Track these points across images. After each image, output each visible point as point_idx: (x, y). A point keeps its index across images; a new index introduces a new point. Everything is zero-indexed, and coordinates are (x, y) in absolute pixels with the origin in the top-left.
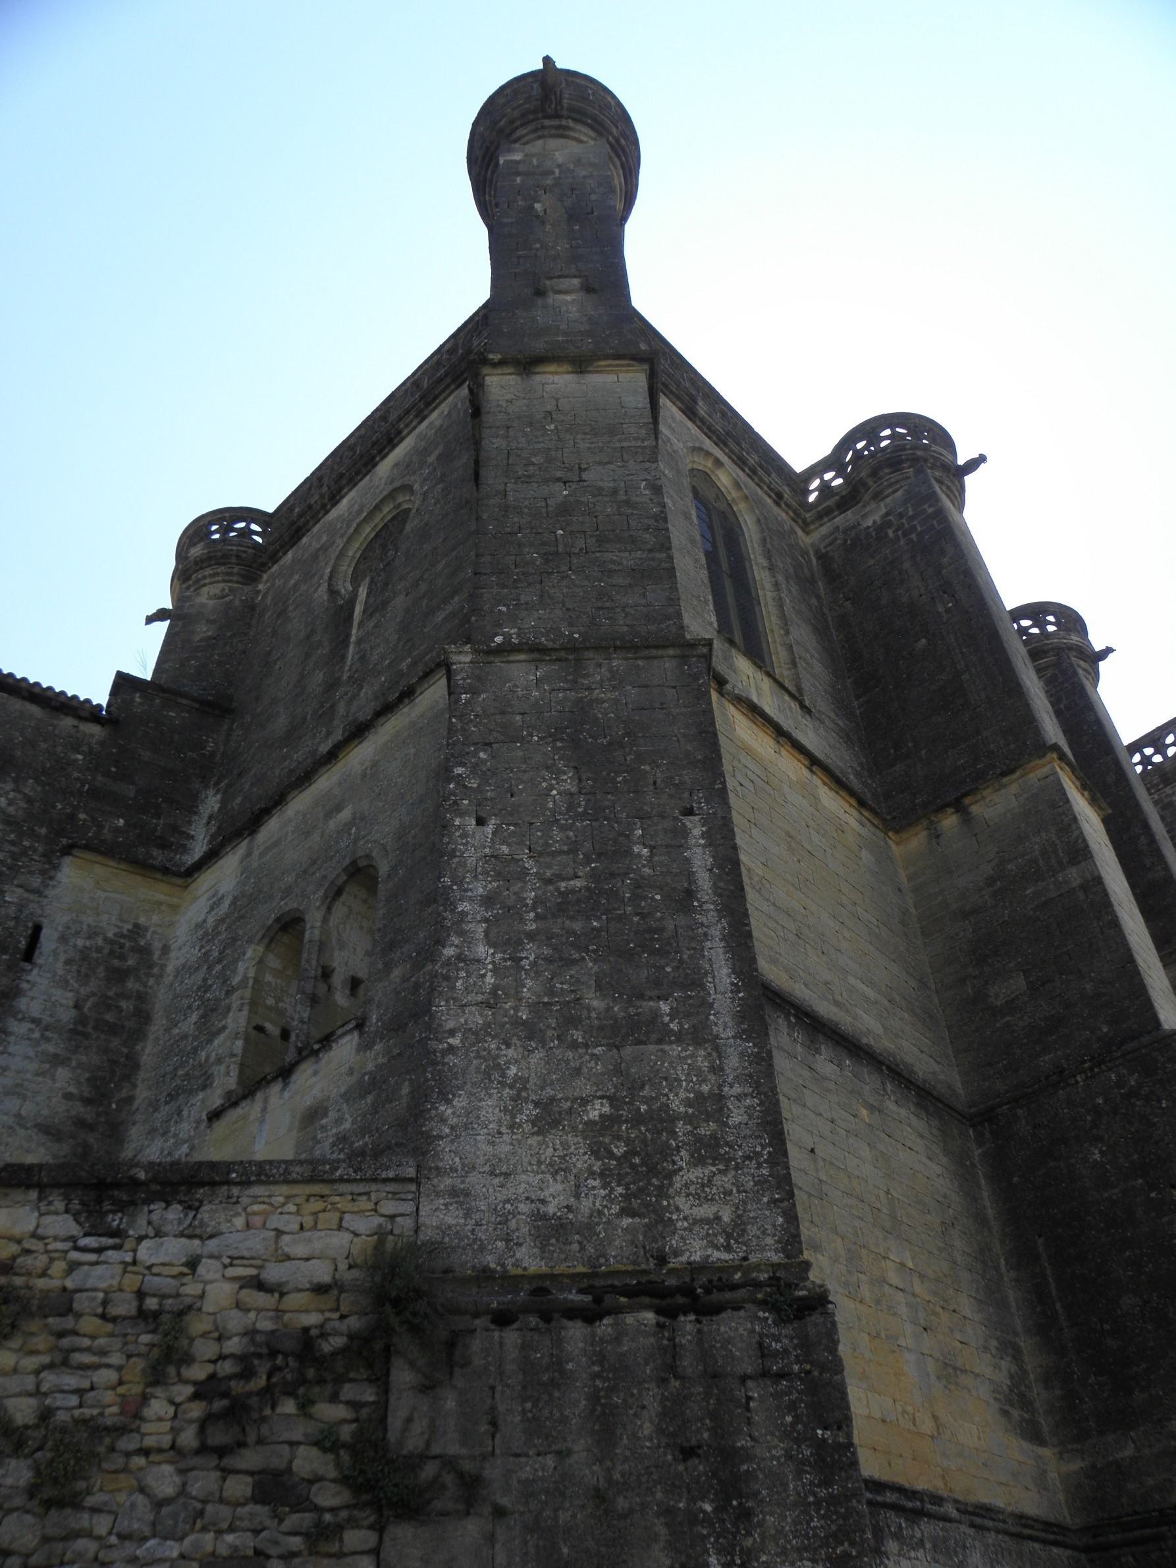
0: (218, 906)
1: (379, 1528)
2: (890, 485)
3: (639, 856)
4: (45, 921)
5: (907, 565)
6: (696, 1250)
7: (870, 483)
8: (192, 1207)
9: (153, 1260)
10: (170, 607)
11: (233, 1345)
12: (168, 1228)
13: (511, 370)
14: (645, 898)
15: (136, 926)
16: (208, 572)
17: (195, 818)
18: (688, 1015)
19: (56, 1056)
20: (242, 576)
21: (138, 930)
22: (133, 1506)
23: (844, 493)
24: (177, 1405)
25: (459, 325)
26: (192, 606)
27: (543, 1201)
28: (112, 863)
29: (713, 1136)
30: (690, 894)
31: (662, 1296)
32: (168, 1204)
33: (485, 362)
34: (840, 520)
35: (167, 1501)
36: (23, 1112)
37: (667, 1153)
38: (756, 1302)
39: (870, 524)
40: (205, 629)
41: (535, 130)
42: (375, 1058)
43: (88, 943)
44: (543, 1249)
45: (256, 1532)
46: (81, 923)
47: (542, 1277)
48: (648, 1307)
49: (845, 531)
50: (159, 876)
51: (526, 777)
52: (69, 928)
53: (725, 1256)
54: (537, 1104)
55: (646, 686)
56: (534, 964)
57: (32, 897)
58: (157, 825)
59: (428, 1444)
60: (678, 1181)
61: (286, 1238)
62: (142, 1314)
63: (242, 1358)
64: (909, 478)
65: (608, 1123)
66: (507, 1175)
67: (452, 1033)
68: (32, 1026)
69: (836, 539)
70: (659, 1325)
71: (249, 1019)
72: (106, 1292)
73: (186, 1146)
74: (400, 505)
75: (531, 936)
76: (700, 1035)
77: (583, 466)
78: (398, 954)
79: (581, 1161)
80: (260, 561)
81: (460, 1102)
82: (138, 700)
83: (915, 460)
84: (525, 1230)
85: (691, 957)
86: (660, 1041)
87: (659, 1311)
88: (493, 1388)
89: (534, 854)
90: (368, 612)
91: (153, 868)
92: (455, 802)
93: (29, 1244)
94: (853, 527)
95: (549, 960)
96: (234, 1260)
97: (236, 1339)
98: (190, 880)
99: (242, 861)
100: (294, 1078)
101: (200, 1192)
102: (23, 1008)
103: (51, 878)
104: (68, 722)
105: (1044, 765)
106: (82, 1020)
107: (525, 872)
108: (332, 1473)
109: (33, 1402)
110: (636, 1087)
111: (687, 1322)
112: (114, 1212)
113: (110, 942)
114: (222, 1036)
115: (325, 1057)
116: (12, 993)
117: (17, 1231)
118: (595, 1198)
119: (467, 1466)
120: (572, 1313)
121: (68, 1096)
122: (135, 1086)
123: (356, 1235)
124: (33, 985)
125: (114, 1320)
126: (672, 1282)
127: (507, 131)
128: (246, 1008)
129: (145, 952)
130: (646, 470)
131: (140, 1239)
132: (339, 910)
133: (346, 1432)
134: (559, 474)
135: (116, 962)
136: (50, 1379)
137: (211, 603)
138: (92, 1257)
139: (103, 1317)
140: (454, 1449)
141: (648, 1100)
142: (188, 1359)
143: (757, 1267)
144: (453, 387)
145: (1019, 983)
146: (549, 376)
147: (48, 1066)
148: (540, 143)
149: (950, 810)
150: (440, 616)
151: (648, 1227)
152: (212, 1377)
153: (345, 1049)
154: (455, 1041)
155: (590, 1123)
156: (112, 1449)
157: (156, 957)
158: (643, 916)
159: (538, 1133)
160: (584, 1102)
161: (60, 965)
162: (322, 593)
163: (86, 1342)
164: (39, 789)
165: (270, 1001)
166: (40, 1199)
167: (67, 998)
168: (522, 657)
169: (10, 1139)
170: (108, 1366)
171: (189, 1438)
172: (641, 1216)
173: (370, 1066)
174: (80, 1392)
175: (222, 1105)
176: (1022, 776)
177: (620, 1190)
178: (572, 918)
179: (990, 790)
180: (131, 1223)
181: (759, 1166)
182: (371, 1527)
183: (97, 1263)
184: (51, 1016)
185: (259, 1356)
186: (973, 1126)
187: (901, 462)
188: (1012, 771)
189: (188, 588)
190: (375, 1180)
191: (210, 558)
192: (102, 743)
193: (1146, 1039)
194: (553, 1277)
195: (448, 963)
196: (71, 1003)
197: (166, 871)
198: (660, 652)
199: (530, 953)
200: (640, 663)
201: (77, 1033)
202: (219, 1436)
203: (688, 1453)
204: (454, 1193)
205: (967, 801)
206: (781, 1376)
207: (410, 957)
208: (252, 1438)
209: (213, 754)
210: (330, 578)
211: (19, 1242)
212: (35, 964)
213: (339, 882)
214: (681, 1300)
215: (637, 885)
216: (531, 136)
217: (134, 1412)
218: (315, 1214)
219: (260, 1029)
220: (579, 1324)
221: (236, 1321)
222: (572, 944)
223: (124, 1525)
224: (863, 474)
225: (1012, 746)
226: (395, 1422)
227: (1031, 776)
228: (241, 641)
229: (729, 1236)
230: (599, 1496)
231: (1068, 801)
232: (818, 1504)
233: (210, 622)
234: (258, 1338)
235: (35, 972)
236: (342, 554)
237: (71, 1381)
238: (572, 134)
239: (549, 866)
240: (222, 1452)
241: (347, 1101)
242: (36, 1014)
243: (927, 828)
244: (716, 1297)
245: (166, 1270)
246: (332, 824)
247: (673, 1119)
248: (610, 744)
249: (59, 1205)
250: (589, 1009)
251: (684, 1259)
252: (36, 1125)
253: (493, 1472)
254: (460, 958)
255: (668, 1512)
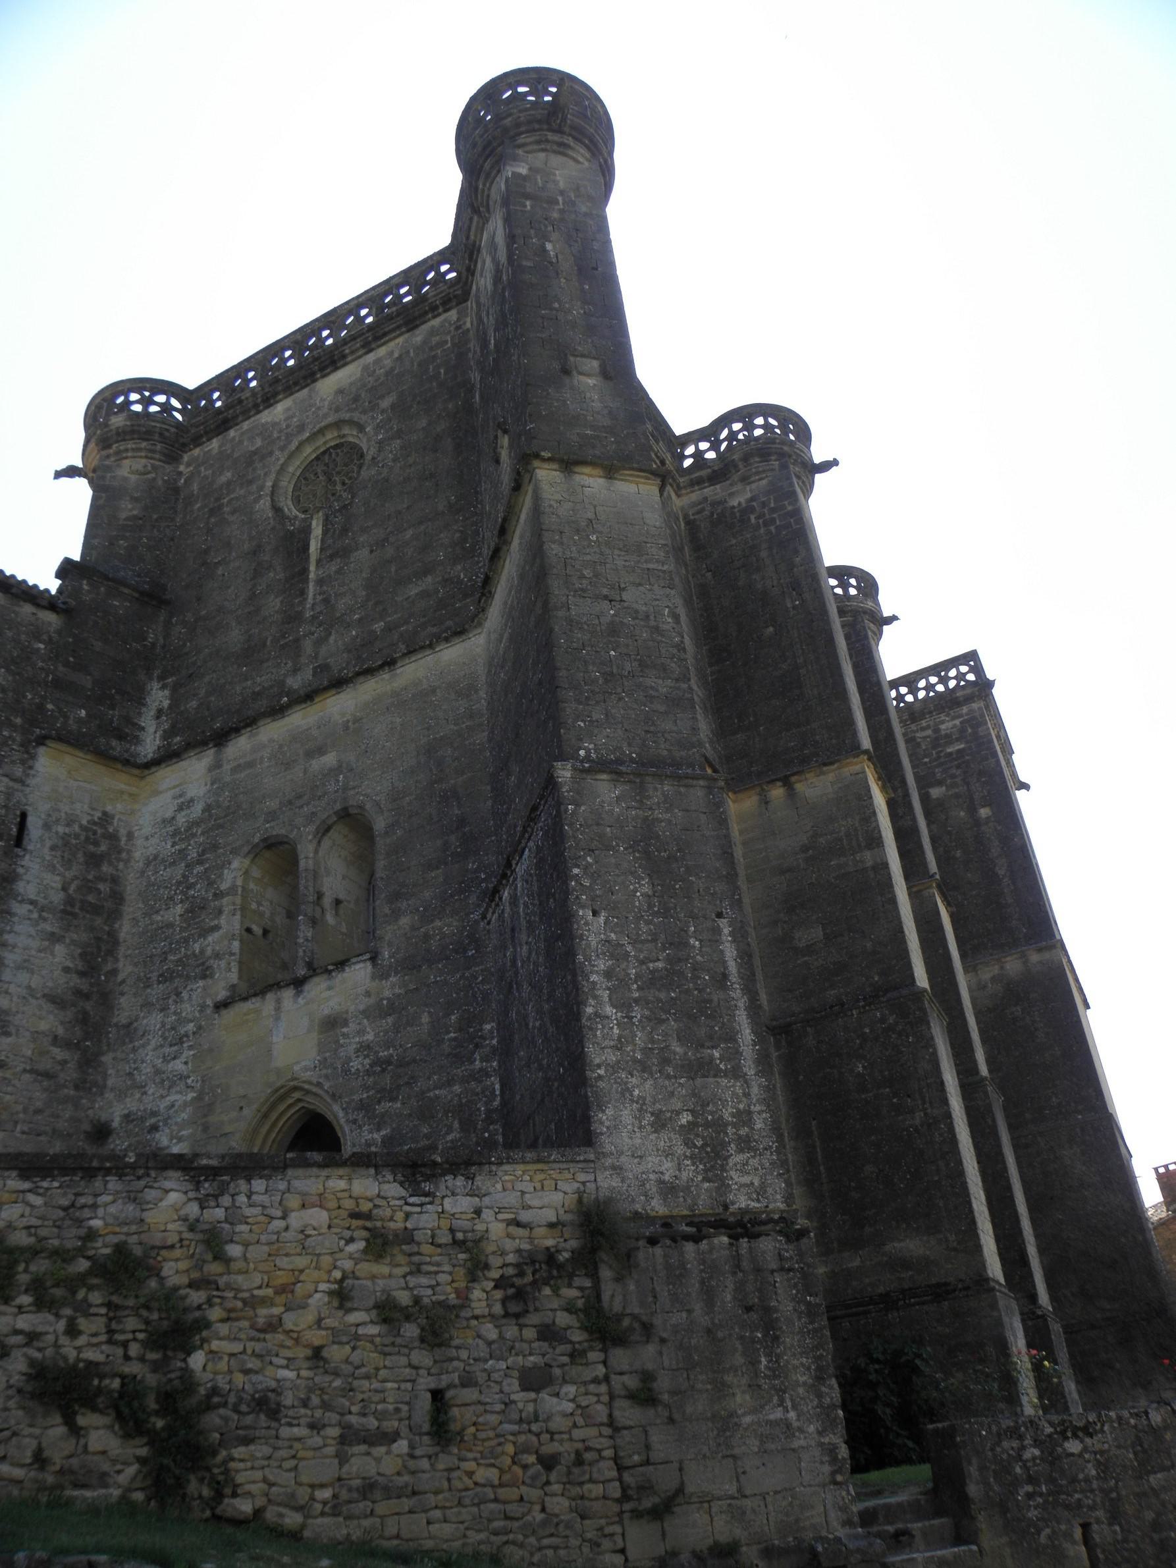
0: (189, 807)
1: (604, 1350)
2: (757, 473)
3: (694, 947)
4: (29, 808)
5: (764, 554)
6: (742, 1201)
7: (741, 466)
8: (470, 1178)
9: (454, 1210)
10: (80, 465)
11: (511, 1258)
12: (458, 1191)
13: (555, 466)
14: (700, 978)
15: (105, 813)
16: (130, 445)
17: (144, 709)
18: (729, 1060)
19: (53, 934)
20: (165, 455)
21: (106, 818)
22: (477, 1345)
23: (716, 468)
24: (487, 1293)
25: (412, 263)
26: (114, 477)
27: (662, 1173)
28: (81, 755)
29: (747, 1136)
30: (725, 976)
31: (731, 1229)
32: (455, 1176)
33: (537, 456)
34: (708, 491)
35: (493, 1342)
36: (33, 985)
37: (724, 1145)
38: (775, 1231)
39: (736, 504)
40: (130, 506)
41: (539, 142)
42: (390, 988)
43: (67, 830)
44: (665, 1200)
45: (544, 1355)
46: (59, 811)
47: (667, 1217)
48: (724, 1234)
49: (713, 504)
50: (119, 766)
51: (620, 880)
52: (49, 815)
53: (757, 1205)
54: (652, 1114)
55: (687, 811)
56: (640, 1021)
57: (17, 786)
58: (113, 716)
59: (624, 1308)
60: (731, 1162)
61: (527, 1196)
62: (455, 1242)
63: (517, 1265)
64: (773, 470)
65: (692, 1125)
66: (641, 1157)
67: (599, 1066)
68: (31, 907)
69: (703, 510)
70: (731, 1244)
71: (242, 923)
72: (432, 1230)
73: (192, 1025)
74: (344, 436)
75: (636, 1001)
76: (736, 1073)
77: (623, 586)
78: (405, 904)
79: (680, 1149)
80: (182, 440)
81: (610, 1112)
82: (86, 587)
83: (782, 455)
84: (654, 1189)
85: (729, 1020)
86: (715, 1076)
87: (730, 1237)
88: (652, 1279)
89: (634, 942)
90: (330, 553)
91: (115, 759)
92: (577, 897)
93: (378, 1202)
94: (720, 503)
95: (649, 1019)
96: (501, 1210)
97: (511, 1255)
98: (147, 772)
99: (210, 770)
100: (307, 987)
101: (473, 1169)
102: (21, 890)
103: (31, 768)
104: (27, 609)
105: (856, 764)
106: (69, 901)
107: (627, 954)
108: (577, 1325)
109: (406, 1293)
110: (705, 1104)
111: (744, 1242)
112: (425, 1181)
113: (84, 828)
114: (216, 935)
115: (339, 977)
116: (10, 878)
117: (369, 1194)
118: (689, 1172)
119: (644, 1318)
120: (687, 1238)
121: (66, 970)
122: (117, 960)
123: (565, 1193)
124: (27, 869)
125: (439, 1246)
126: (731, 1219)
127: (512, 133)
128: (239, 913)
129: (113, 837)
130: (667, 596)
131: (443, 1197)
132: (326, 843)
133: (580, 1303)
134: (605, 591)
135: (91, 848)
136: (412, 1281)
137: (133, 477)
138: (418, 1209)
139: (432, 1244)
140: (637, 1311)
141: (712, 1113)
142: (487, 1266)
143: (773, 1211)
144: (404, 329)
145: (817, 933)
146: (586, 478)
147: (47, 943)
148: (542, 155)
149: (779, 784)
150: (413, 591)
151: (718, 1189)
152: (502, 1276)
153: (359, 973)
154: (601, 1072)
155: (682, 1126)
156: (457, 1316)
157: (123, 843)
158: (700, 991)
159: (655, 1132)
160: (678, 1113)
161: (46, 851)
162: (264, 505)
163: (428, 1259)
164: (10, 678)
165: (254, 906)
166: (377, 1174)
167: (55, 881)
168: (604, 776)
169: (25, 1009)
170: (443, 1272)
171: (498, 1309)
172: (713, 1182)
173: (387, 993)
174: (432, 1287)
175: (228, 998)
176: (839, 768)
177: (701, 1167)
178: (659, 990)
179: (812, 774)
180: (437, 1188)
181: (772, 1154)
182: (600, 1350)
183: (421, 1213)
184: (45, 898)
185: (526, 1264)
186: (774, 1035)
187: (770, 454)
188: (832, 763)
189: (108, 457)
190: (572, 1162)
191: (133, 432)
192: (59, 632)
193: (905, 992)
194: (672, 1217)
195: (589, 1019)
196: (60, 886)
197: (127, 763)
198: (695, 782)
199: (637, 1013)
200: (682, 789)
201: (69, 912)
202: (514, 1308)
203: (748, 1309)
204: (613, 1167)
205: (793, 779)
206: (790, 1270)
207: (417, 910)
208: (531, 1309)
209: (153, 645)
210: (272, 493)
211: (371, 1200)
212: (25, 850)
213: (330, 822)
214: (739, 1230)
215: (694, 969)
216: (535, 147)
217: (464, 1297)
218: (541, 1181)
219: (249, 930)
220: (691, 1244)
221: (509, 1245)
222: (661, 1008)
223: (476, 1355)
224: (736, 457)
225: (834, 741)
226: (605, 1297)
227: (846, 770)
228: (168, 527)
229: (758, 1194)
230: (709, 1331)
231: (871, 797)
232: (809, 1332)
233: (135, 500)
234: (525, 1254)
235: (27, 857)
236: (282, 469)
237: (424, 1281)
238: (570, 153)
239: (641, 951)
240: (517, 1316)
241: (368, 1018)
242: (32, 897)
243: (760, 795)
244: (757, 1229)
245: (464, 1216)
246: (317, 764)
247: (726, 1125)
248: (669, 858)
249: (390, 1177)
250: (675, 1053)
251: (736, 1206)
252: (44, 996)
253: (657, 1321)
254: (596, 1014)
255: (741, 1338)
